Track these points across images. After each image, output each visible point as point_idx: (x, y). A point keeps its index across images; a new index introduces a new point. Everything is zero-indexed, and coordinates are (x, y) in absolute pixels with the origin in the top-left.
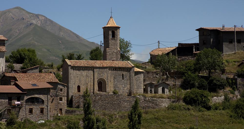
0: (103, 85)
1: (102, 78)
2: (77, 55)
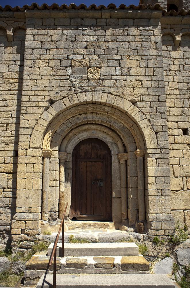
0: (115, 166)
1: (103, 98)
2: (188, 248)
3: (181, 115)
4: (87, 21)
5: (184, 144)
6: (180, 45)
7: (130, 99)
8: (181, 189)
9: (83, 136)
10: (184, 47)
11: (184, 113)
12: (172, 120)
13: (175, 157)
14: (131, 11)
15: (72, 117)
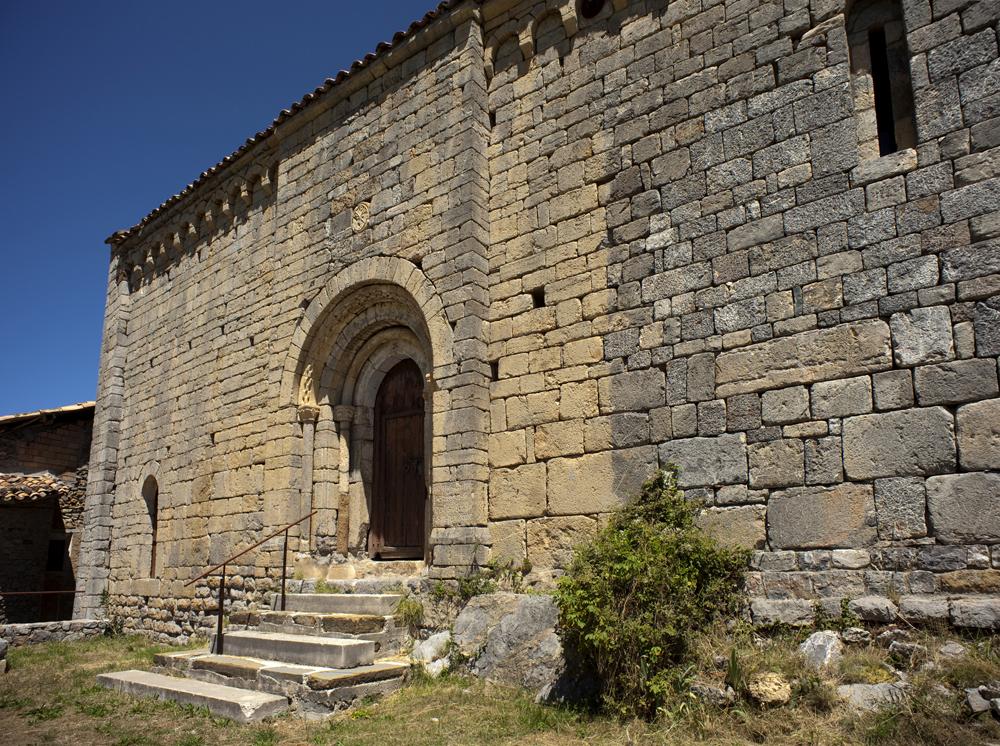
3: (531, 254)
4: (356, 100)
5: (532, 333)
6: (536, 53)
7: (410, 256)
8: (521, 461)
9: (380, 360)
10: (544, 54)
11: (537, 246)
12: (510, 275)
13: (511, 376)
14: (414, 38)
15: (345, 324)
